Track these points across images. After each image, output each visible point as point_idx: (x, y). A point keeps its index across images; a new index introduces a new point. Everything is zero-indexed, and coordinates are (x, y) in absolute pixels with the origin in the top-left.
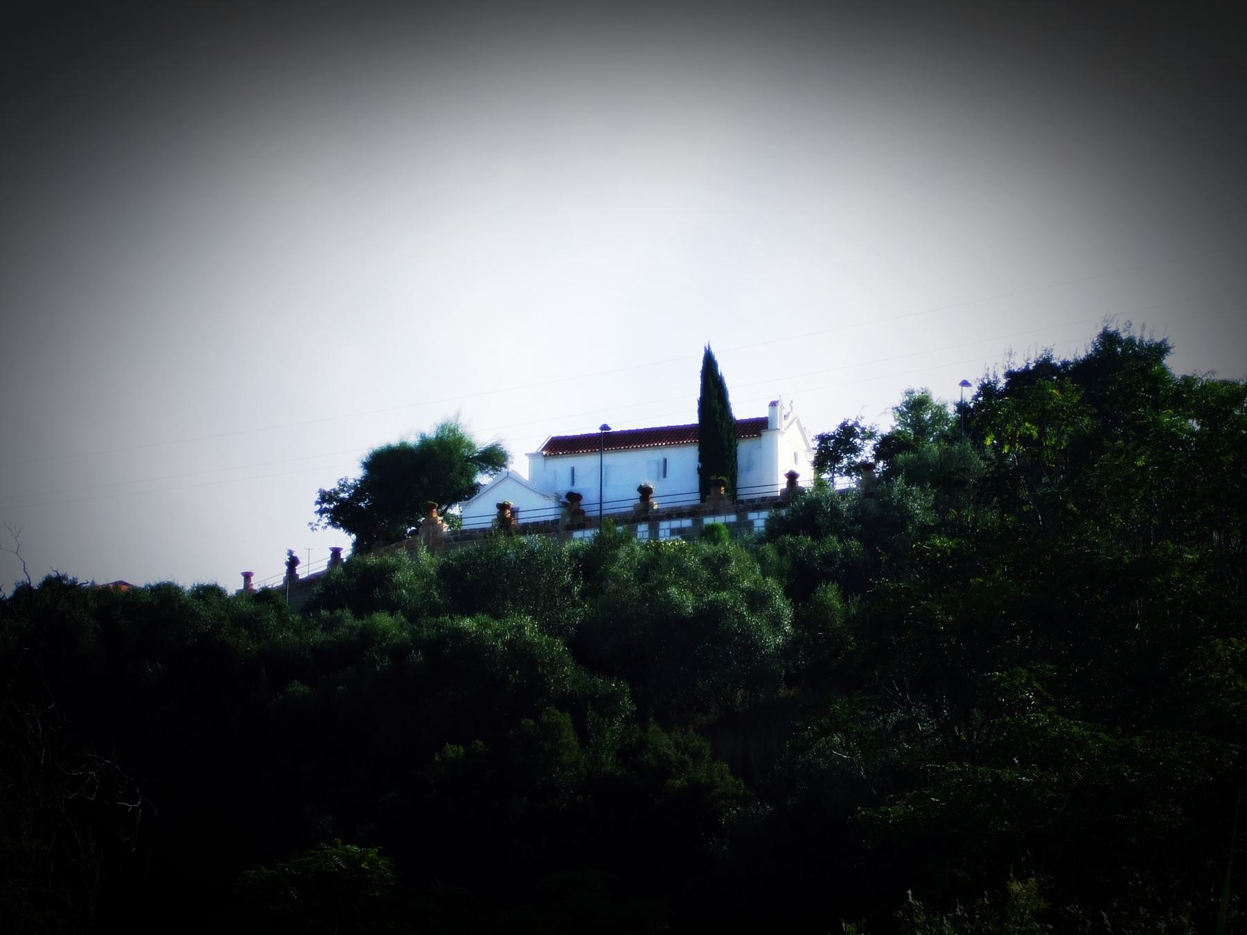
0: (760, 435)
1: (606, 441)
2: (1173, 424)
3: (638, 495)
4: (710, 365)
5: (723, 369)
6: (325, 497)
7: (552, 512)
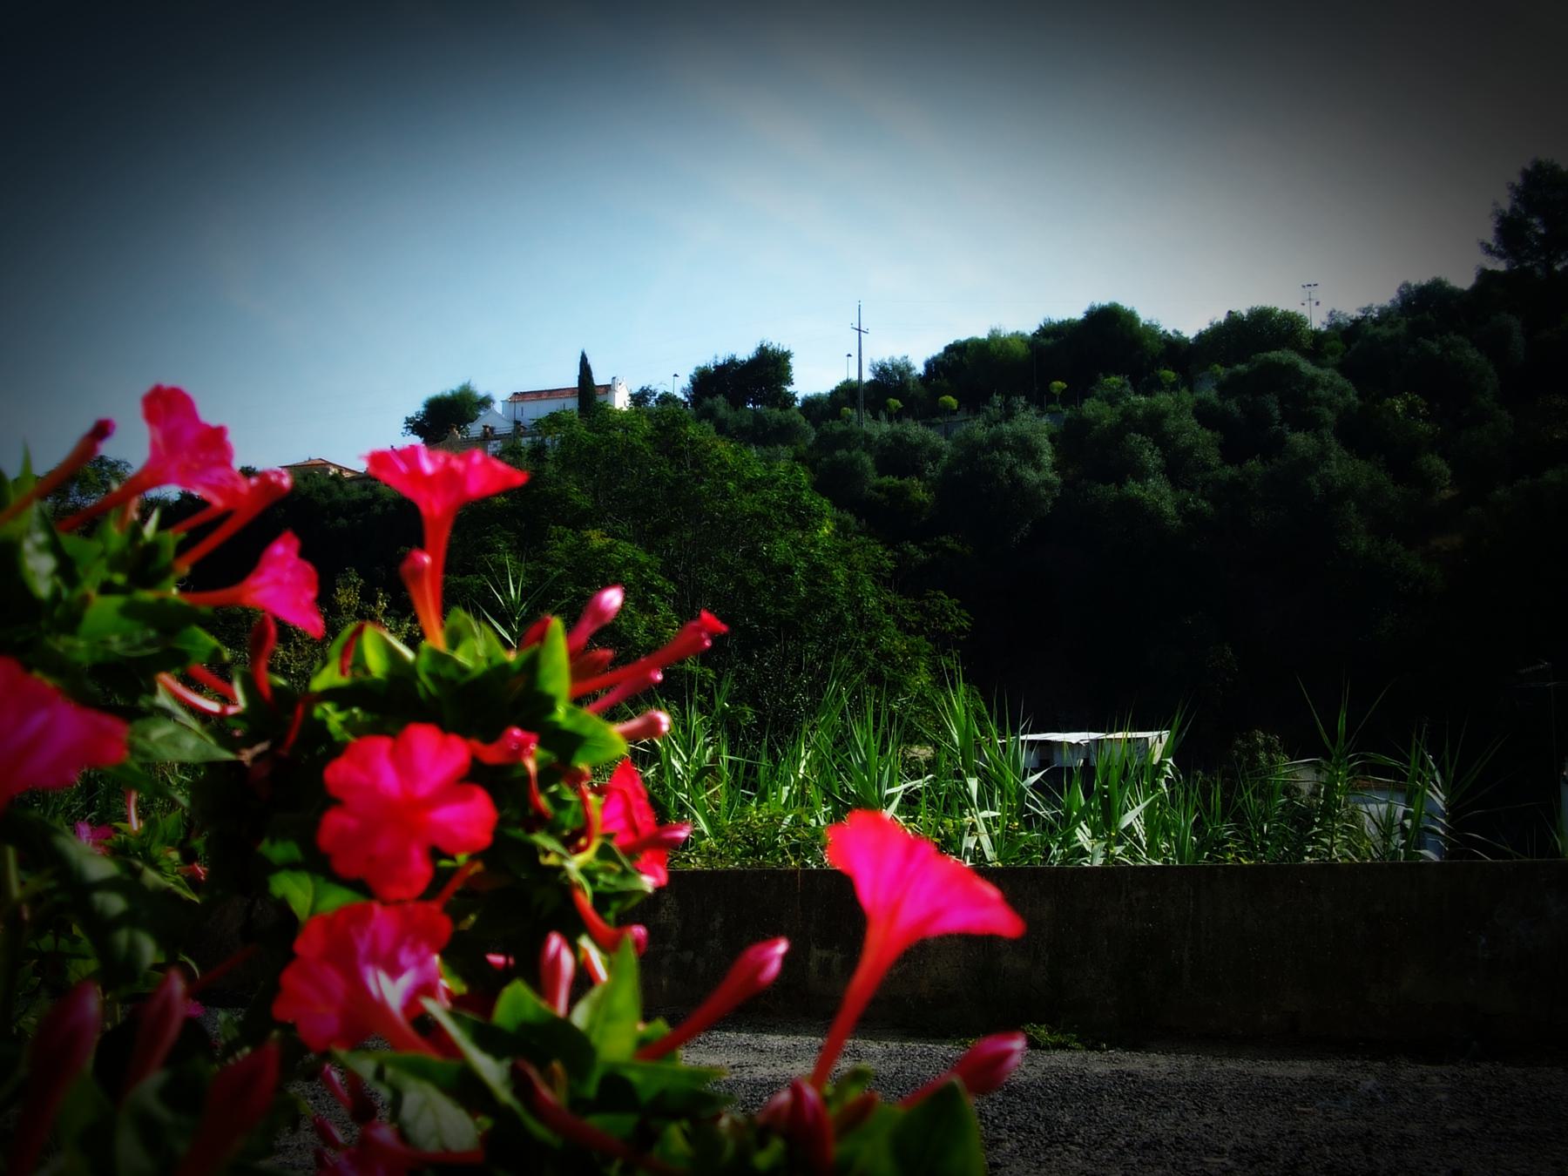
1: (538, 395)
2: (419, 572)
4: (584, 360)
5: (590, 361)
6: (408, 420)
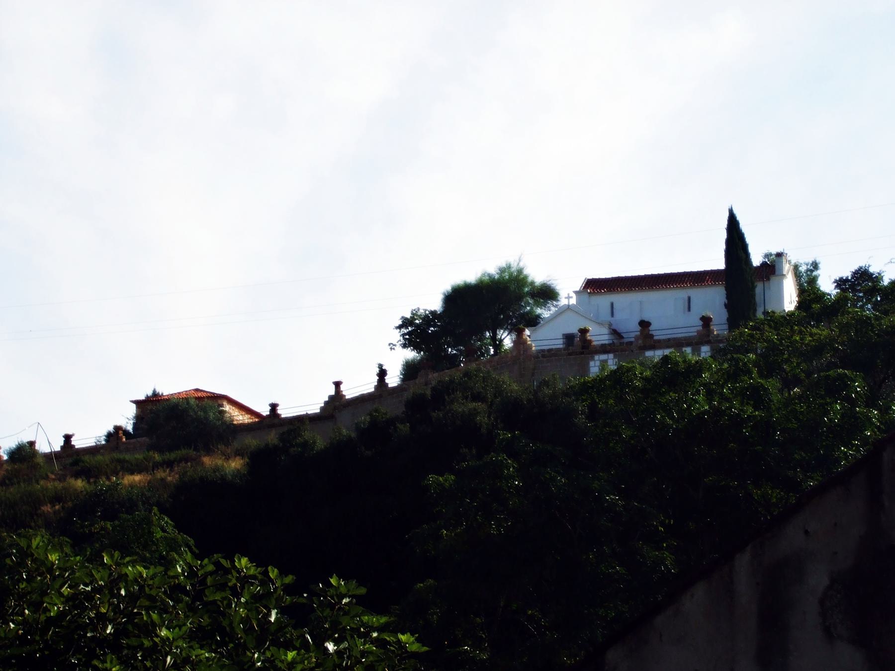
0: (768, 279)
3: (701, 323)
4: (733, 224)
5: (744, 227)
7: (606, 337)
